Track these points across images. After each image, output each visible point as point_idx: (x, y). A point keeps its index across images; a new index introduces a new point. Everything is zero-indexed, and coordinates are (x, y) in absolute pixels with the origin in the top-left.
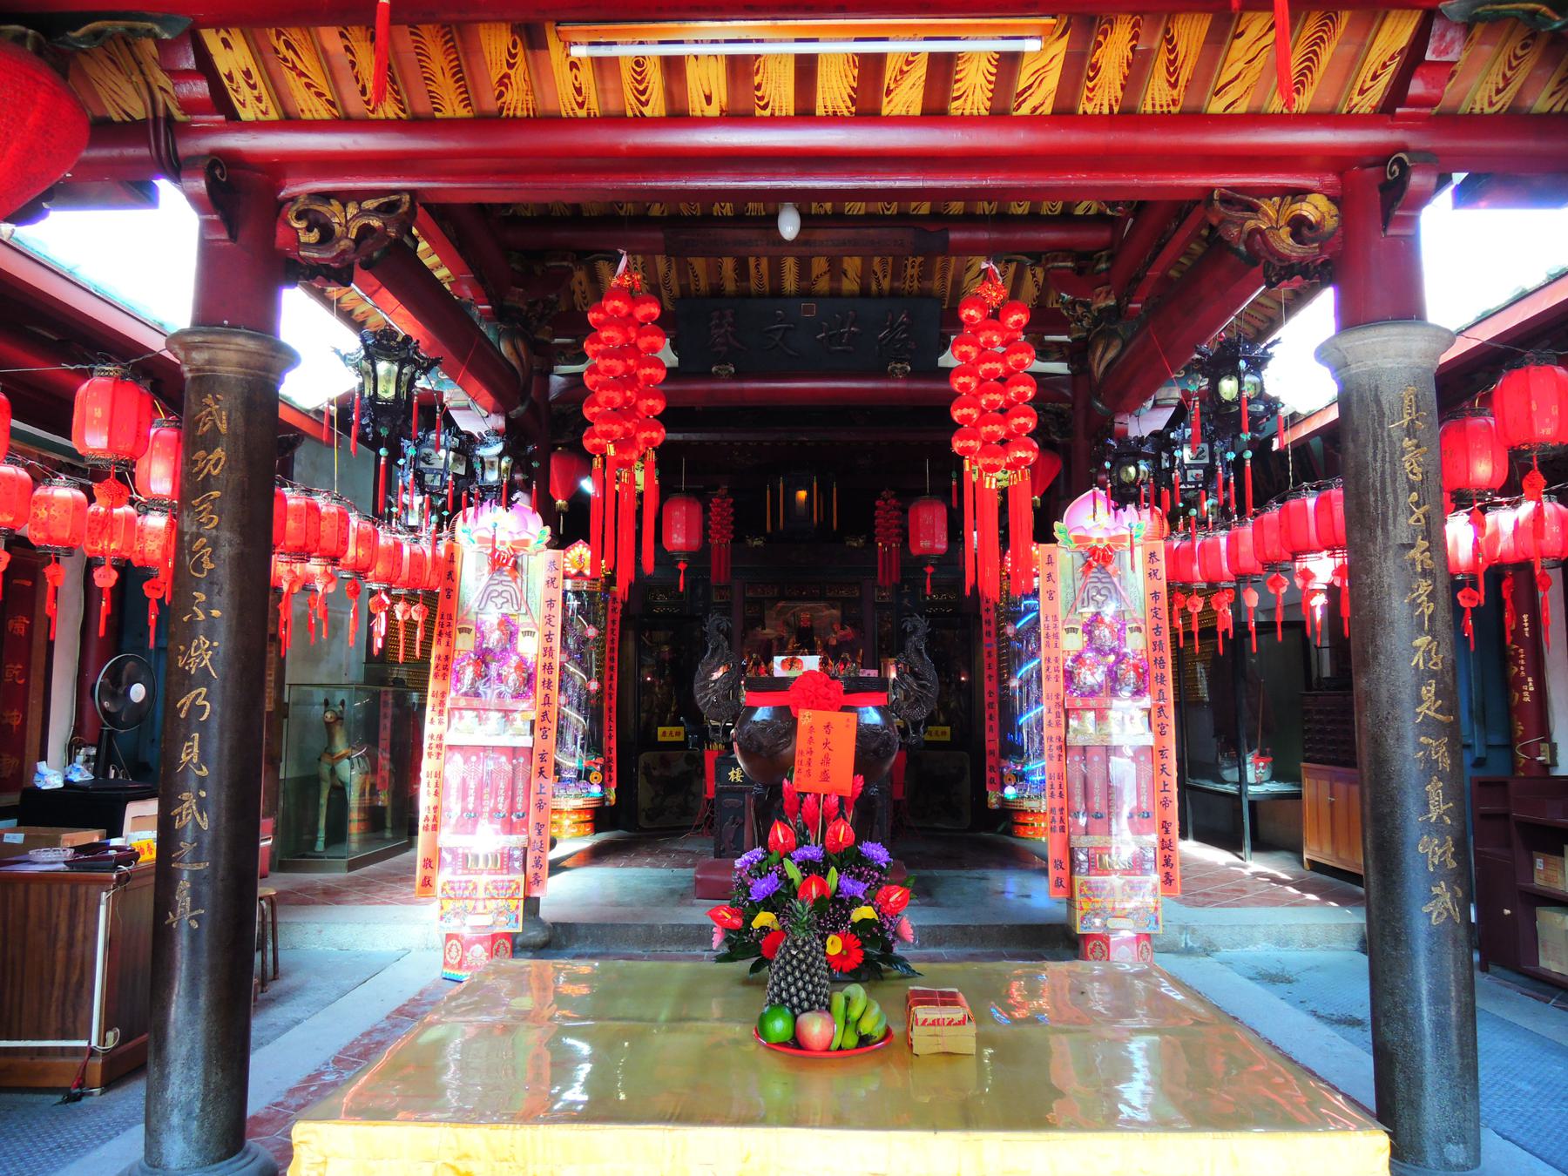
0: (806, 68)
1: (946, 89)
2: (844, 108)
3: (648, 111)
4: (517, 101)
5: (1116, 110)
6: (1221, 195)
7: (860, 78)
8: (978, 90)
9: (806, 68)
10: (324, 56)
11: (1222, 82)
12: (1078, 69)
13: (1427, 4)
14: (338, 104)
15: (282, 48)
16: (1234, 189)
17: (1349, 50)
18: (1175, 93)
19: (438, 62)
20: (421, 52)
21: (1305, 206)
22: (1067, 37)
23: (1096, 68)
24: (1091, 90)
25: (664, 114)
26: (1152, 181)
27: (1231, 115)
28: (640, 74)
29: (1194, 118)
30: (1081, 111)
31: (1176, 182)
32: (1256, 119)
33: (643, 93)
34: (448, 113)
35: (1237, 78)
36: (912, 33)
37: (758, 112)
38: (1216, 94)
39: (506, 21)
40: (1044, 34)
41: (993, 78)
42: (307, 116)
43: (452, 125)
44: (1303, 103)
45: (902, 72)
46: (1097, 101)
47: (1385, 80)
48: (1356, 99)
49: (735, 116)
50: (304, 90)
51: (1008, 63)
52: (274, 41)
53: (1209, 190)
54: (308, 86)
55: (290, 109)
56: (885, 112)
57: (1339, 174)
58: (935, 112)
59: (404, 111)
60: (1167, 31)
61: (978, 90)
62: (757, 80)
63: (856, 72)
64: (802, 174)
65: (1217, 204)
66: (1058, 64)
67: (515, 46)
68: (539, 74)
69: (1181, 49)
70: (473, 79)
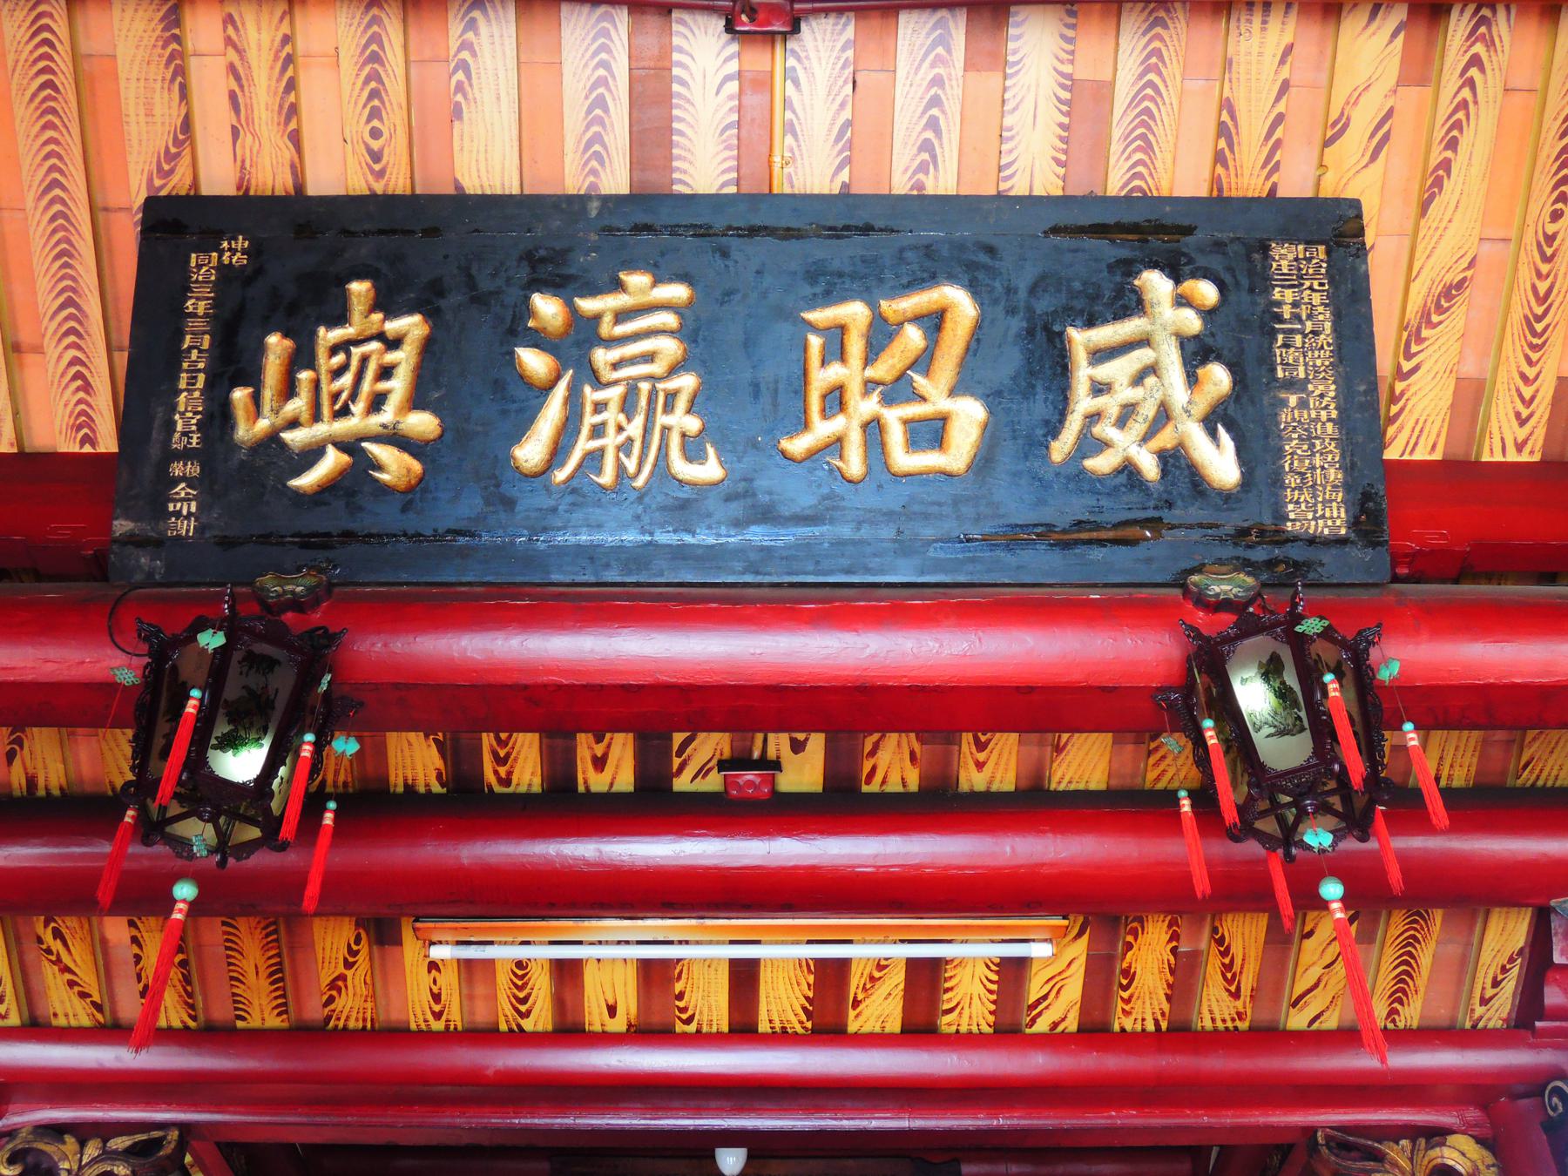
0: (744, 977)
1: (934, 1000)
2: (797, 1022)
3: (528, 1025)
4: (351, 1008)
5: (1164, 1025)
6: (1328, 1138)
7: (817, 986)
8: (976, 999)
9: (744, 977)
10: (102, 951)
11: (1298, 991)
12: (1105, 977)
13: (1538, 901)
14: (107, 1008)
15: (48, 937)
16: (1343, 1128)
17: (1453, 950)
18: (1239, 1004)
19: (253, 958)
20: (231, 946)
21: (1446, 1152)
22: (1086, 937)
23: (1129, 974)
24: (1127, 1001)
25: (550, 1028)
26: (1229, 1118)
27: (1319, 1033)
28: (521, 978)
29: (1269, 1036)
30: (1117, 1028)
31: (1262, 1120)
32: (1347, 1037)
33: (524, 1001)
34: (254, 1022)
35: (1316, 986)
36: (883, 934)
37: (680, 1028)
38: (1294, 1005)
39: (350, 915)
40: (1055, 936)
41: (994, 987)
42: (61, 1022)
43: (259, 1038)
44: (1411, 1015)
45: (872, 979)
46: (1137, 1014)
47: (1510, 986)
48: (1479, 1010)
49: (646, 1033)
50: (64, 989)
51: (1012, 972)
52: (40, 929)
53: (1310, 1131)
54: (71, 984)
55: (39, 1012)
56: (852, 1028)
57: (1483, 1107)
58: (919, 1029)
59: (194, 1018)
60: (1215, 930)
61: (976, 999)
62: (678, 987)
63: (811, 979)
64: (739, 1110)
65: (1324, 1150)
66: (1078, 970)
67: (357, 942)
68: (386, 974)
69: (1237, 950)
70: (296, 980)
